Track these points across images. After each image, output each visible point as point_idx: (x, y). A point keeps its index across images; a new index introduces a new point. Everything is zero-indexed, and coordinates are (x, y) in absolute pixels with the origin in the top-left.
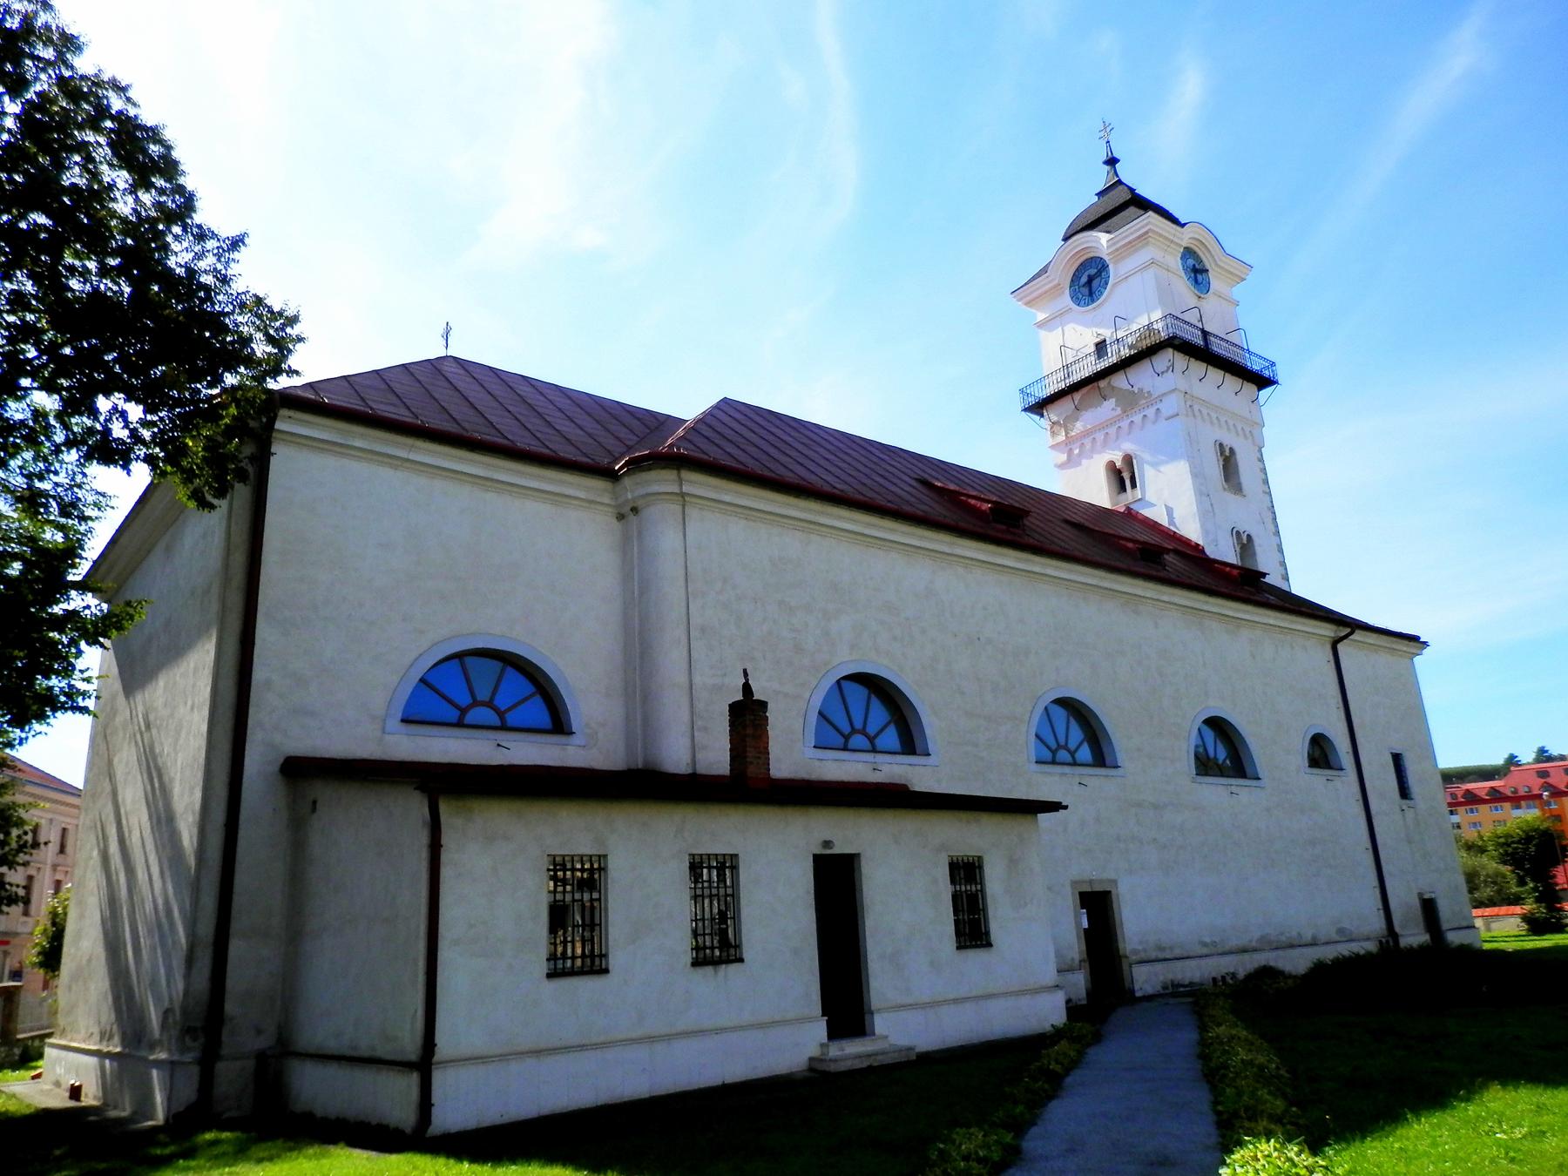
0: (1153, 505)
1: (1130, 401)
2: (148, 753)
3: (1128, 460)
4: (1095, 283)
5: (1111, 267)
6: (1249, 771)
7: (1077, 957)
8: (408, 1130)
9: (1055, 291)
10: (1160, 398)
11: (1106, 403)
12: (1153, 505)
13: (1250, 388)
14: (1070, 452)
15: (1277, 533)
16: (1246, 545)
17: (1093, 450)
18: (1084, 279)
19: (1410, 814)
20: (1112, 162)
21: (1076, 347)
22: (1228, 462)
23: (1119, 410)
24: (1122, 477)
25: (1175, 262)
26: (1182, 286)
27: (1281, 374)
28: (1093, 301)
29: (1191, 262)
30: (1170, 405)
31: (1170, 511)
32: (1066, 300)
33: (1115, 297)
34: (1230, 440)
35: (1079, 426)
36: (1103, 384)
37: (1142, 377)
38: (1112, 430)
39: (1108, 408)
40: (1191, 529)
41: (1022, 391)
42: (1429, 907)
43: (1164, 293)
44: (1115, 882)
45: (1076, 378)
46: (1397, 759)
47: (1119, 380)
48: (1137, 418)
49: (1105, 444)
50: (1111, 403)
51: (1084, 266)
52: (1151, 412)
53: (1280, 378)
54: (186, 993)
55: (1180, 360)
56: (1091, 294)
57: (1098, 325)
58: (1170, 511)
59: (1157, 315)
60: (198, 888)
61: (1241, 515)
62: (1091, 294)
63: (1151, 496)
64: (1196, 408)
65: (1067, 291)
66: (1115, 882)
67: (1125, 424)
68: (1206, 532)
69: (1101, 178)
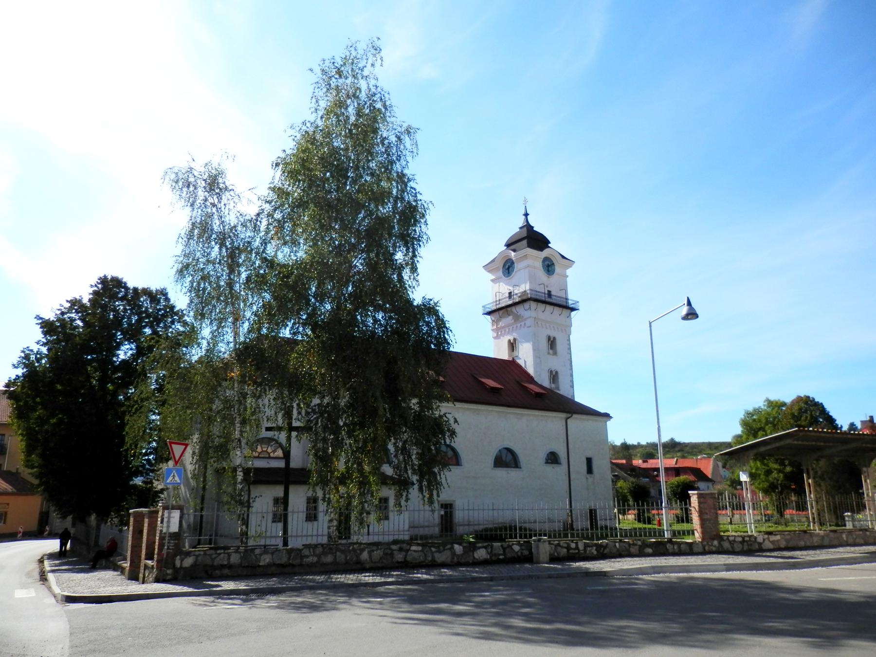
0: (520, 359)
1: (517, 318)
2: (481, 624)
3: (515, 340)
4: (511, 269)
5: (515, 264)
6: (519, 466)
7: (437, 523)
8: (532, 343)
9: (496, 269)
10: (526, 319)
11: (509, 317)
12: (520, 359)
13: (565, 312)
14: (498, 333)
15: (571, 369)
16: (554, 376)
17: (505, 334)
18: (507, 267)
19: (590, 480)
20: (526, 215)
21: (503, 292)
22: (552, 343)
23: (513, 321)
24: (512, 346)
25: (539, 264)
26: (541, 274)
27: (581, 306)
28: (509, 276)
29: (547, 263)
30: (529, 322)
31: (525, 362)
32: (500, 273)
33: (517, 275)
34: (553, 334)
35: (501, 324)
36: (509, 309)
37: (520, 309)
38: (511, 328)
39: (509, 320)
40: (531, 370)
41: (483, 307)
42: (592, 513)
43: (532, 279)
44: (455, 501)
45: (500, 306)
46: (589, 461)
47: (513, 309)
48: (519, 325)
49: (509, 333)
50: (511, 317)
51: (507, 261)
52: (523, 323)
53: (580, 308)
54: (194, 521)
55: (533, 305)
56: (509, 273)
57: (510, 286)
58: (525, 362)
59: (528, 287)
60: (776, 647)
61: (553, 363)
62: (509, 273)
63: (520, 356)
64: (539, 323)
65: (501, 270)
66: (455, 501)
67: (515, 326)
68: (536, 371)
69: (521, 222)
